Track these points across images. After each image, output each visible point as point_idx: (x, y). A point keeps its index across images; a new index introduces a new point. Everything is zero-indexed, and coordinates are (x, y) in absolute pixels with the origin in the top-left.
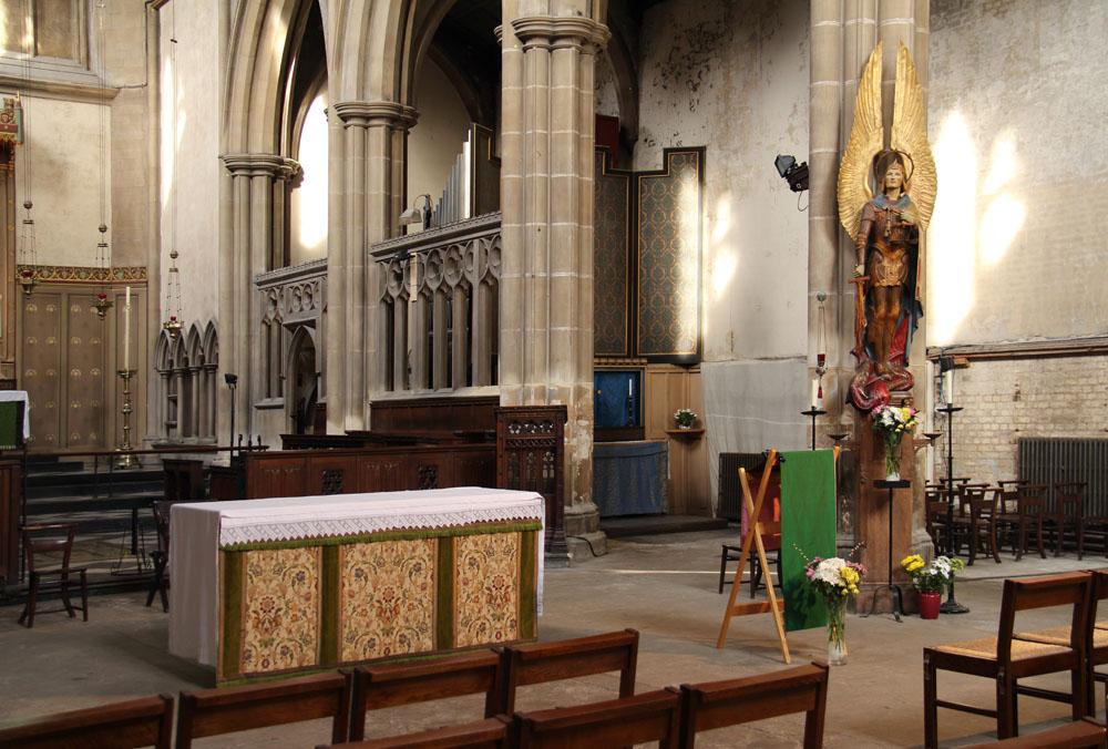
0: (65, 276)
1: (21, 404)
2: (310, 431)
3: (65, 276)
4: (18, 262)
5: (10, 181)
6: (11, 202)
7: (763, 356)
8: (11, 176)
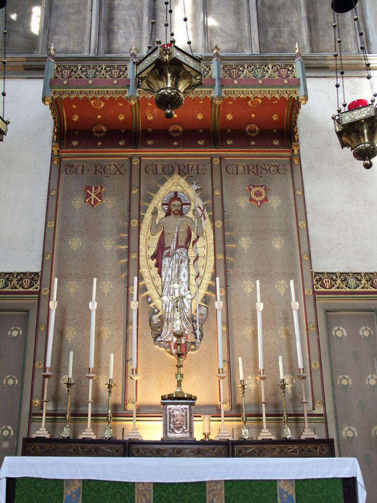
0: (327, 285)
1: (349, 484)
2: (66, 433)
3: (327, 285)
4: (316, 269)
5: (296, 169)
6: (299, 193)
7: (105, 316)
8: (296, 162)
